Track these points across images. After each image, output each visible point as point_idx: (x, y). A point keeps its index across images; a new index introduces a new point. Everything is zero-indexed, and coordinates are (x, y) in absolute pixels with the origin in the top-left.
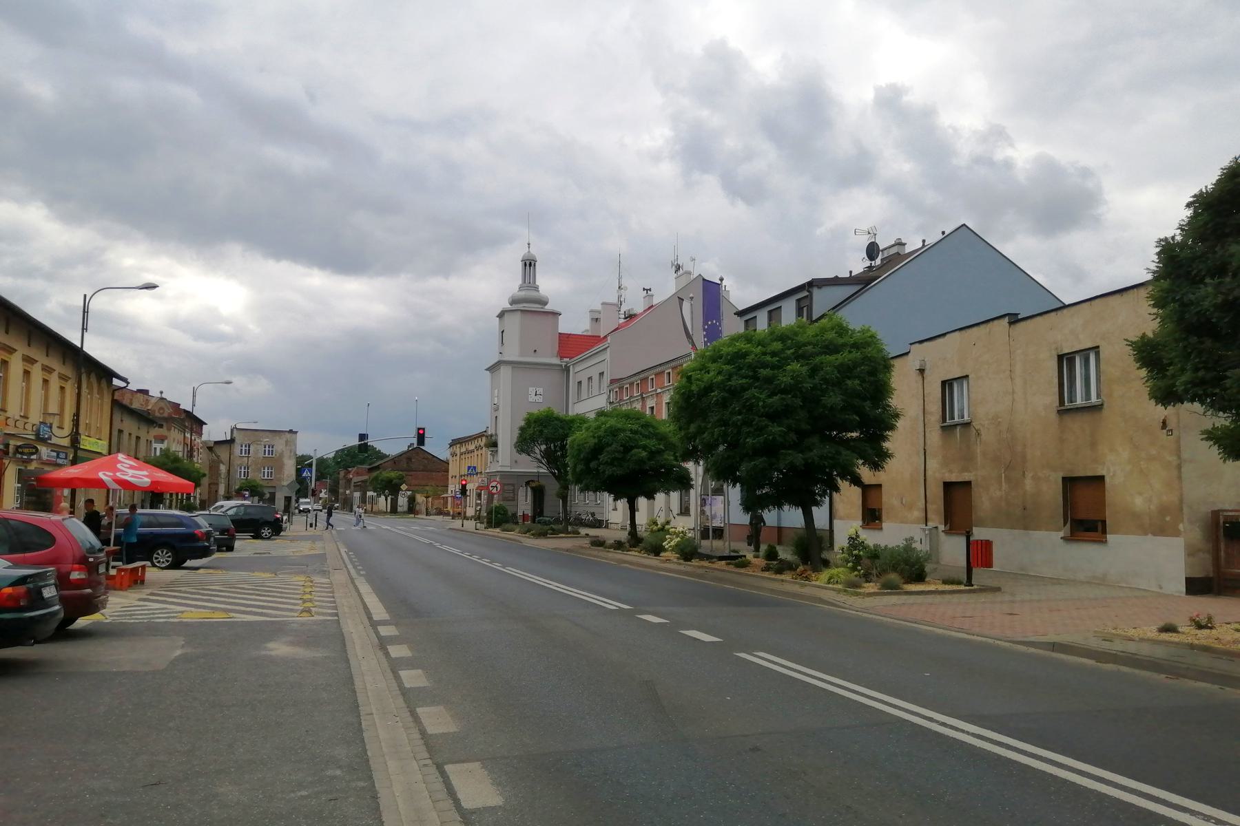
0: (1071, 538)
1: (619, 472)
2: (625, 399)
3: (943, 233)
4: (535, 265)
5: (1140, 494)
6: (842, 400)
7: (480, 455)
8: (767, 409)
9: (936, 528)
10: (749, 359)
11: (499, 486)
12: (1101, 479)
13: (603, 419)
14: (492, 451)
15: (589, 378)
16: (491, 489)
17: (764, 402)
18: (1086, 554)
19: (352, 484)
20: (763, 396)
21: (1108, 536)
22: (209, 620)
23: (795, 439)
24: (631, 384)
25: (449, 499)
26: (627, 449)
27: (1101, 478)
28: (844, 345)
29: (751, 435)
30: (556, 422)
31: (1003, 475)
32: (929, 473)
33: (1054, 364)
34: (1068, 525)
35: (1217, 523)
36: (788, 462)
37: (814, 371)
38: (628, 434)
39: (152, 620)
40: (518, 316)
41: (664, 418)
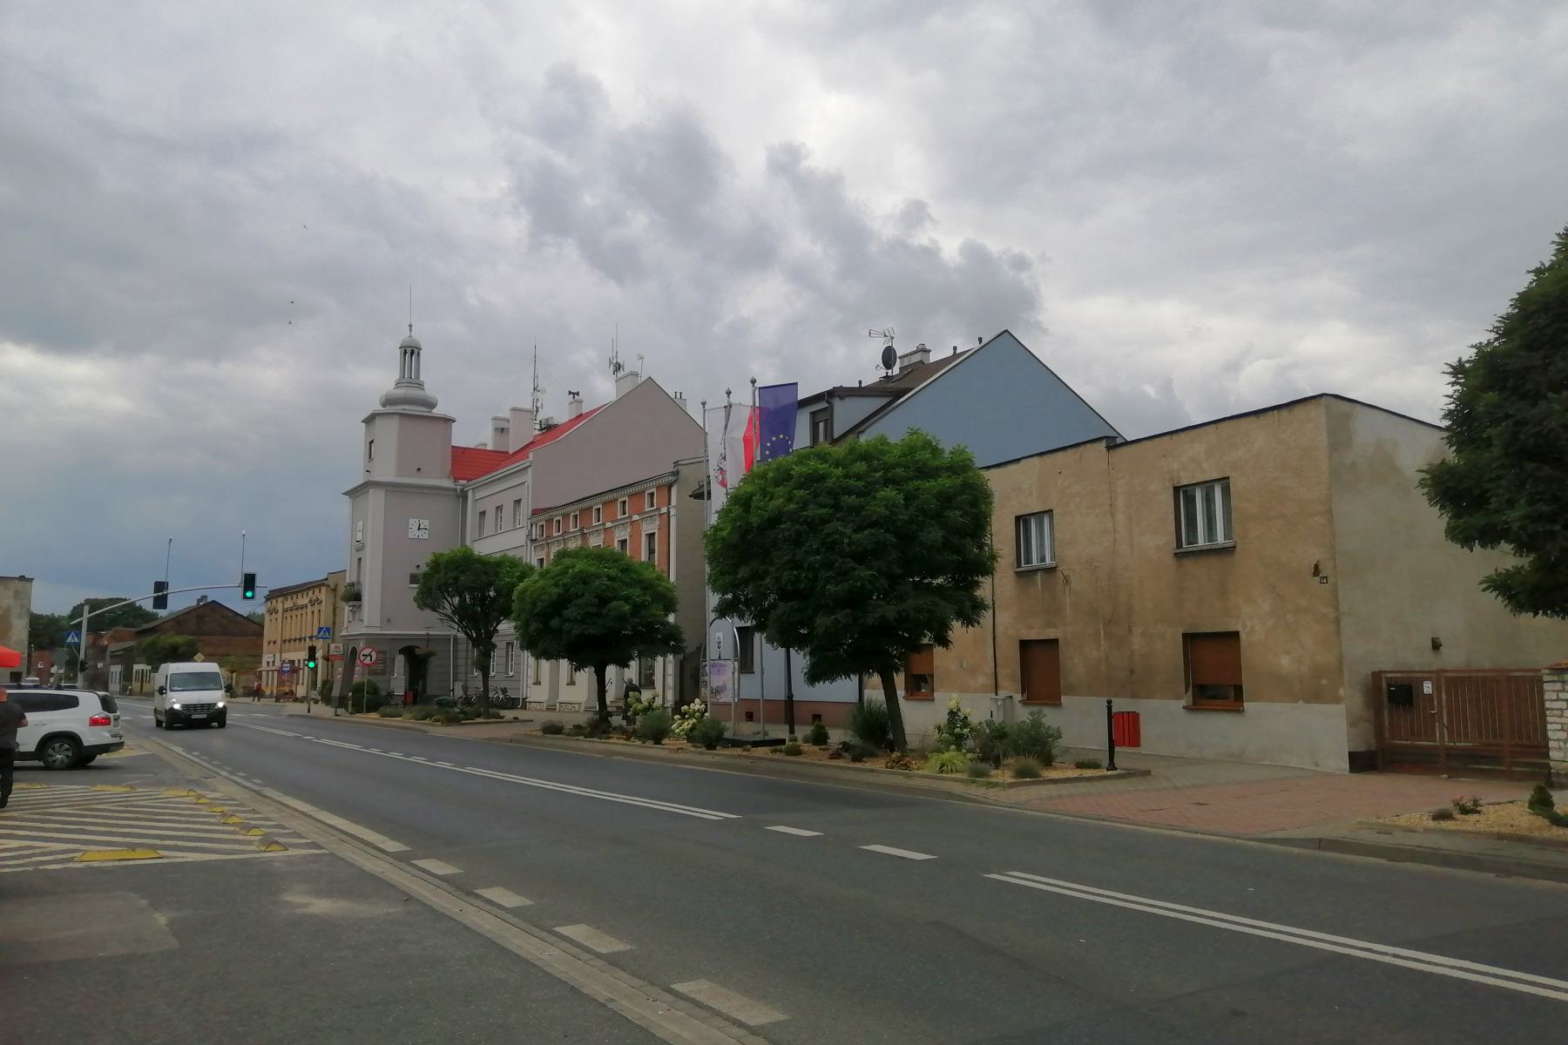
0: (1193, 708)
1: (592, 631)
2: (554, 535)
3: (980, 340)
4: (418, 354)
5: (1287, 653)
6: (942, 537)
7: (316, 612)
8: (854, 547)
9: (1011, 697)
10: (829, 483)
11: (374, 654)
12: (1234, 636)
13: (567, 561)
14: (353, 606)
15: (497, 508)
16: (362, 658)
17: (850, 538)
18: (1216, 728)
19: (108, 654)
20: (848, 531)
21: (1245, 704)
22: (131, 863)
23: (886, 586)
24: (566, 516)
25: (264, 673)
26: (603, 601)
27: (1236, 634)
28: (938, 469)
29: (832, 581)
30: (478, 565)
31: (1102, 631)
32: (999, 629)
33: (1167, 498)
34: (1190, 692)
35: (1380, 689)
36: (880, 615)
37: (909, 498)
38: (605, 581)
39: (42, 867)
40: (395, 422)
41: (643, 560)
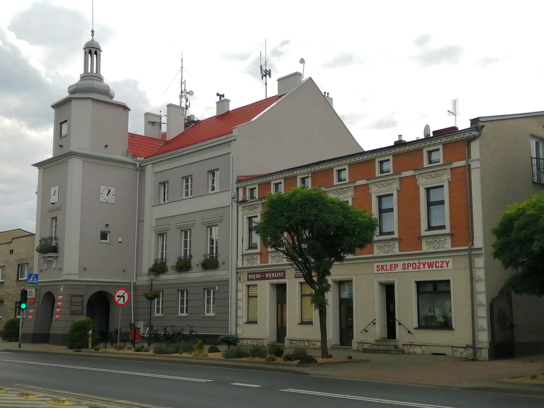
16: (117, 299)
